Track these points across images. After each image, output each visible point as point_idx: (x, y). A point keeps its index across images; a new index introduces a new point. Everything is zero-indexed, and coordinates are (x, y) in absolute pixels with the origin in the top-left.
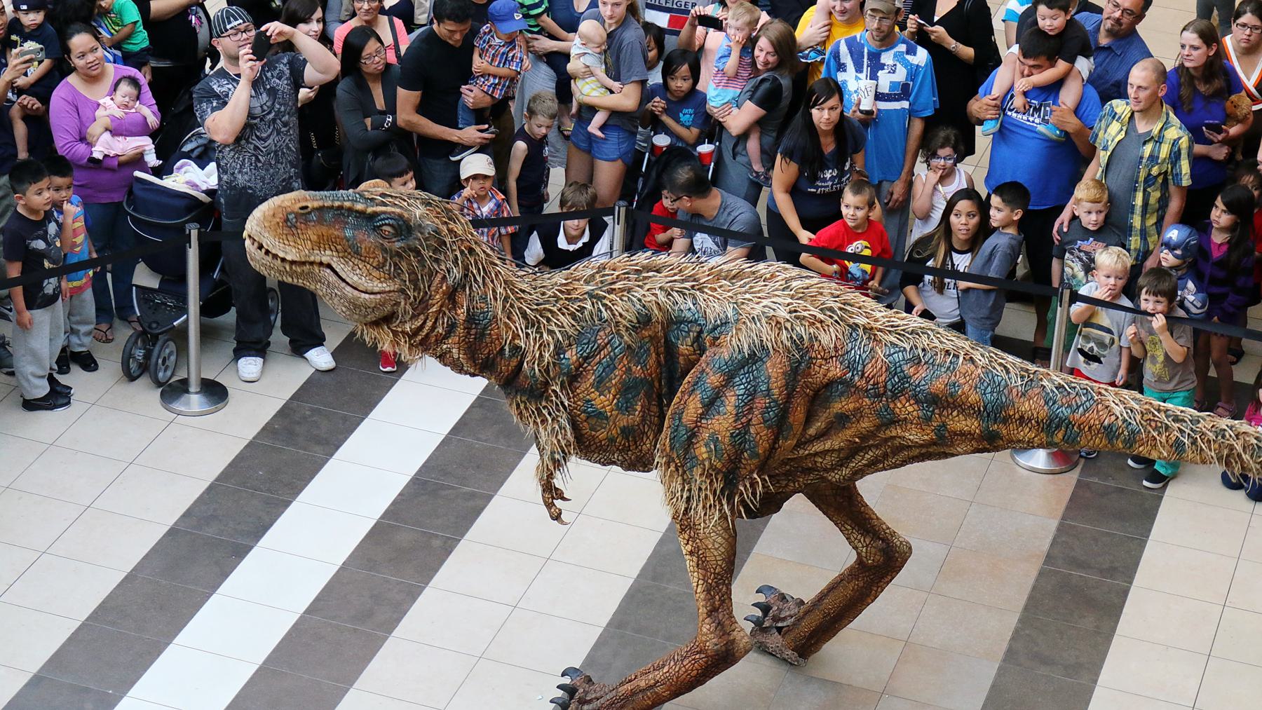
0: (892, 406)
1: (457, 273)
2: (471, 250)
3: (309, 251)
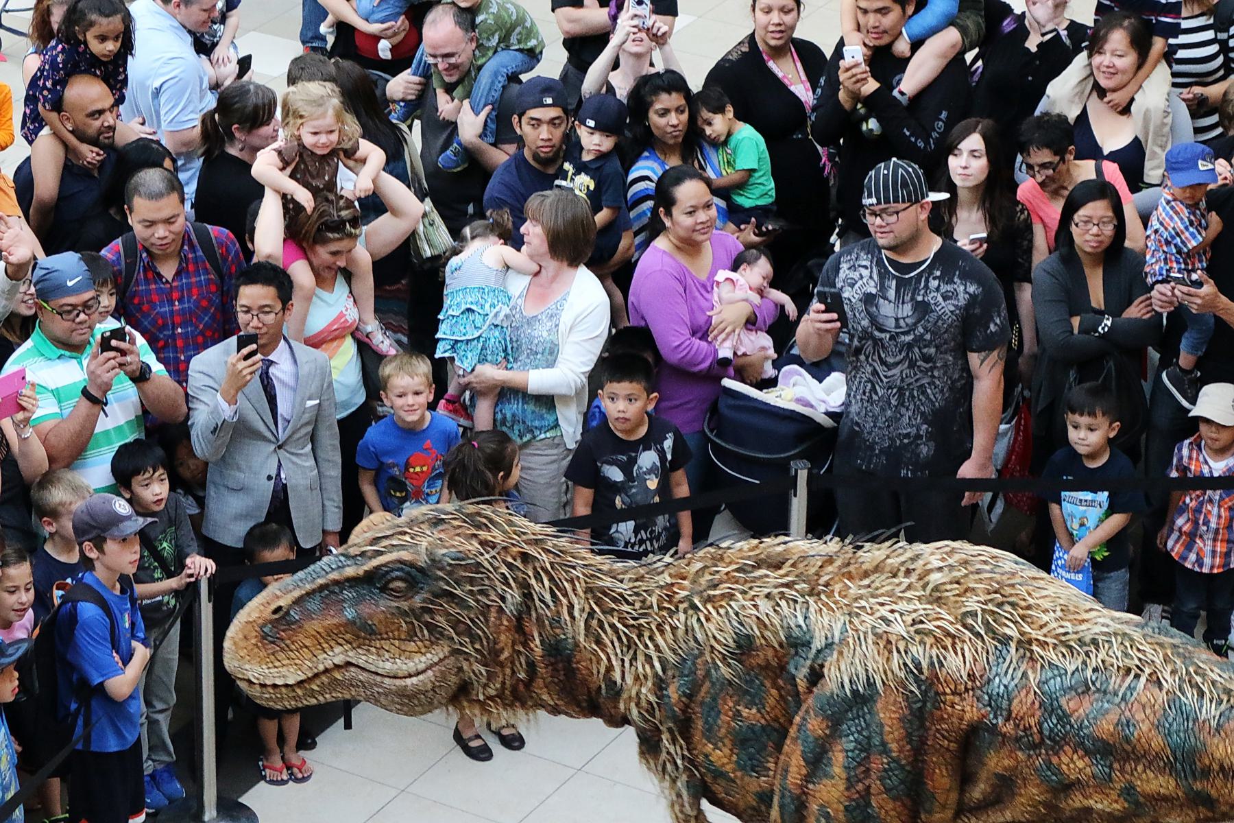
0: (1055, 760)
1: (514, 596)
2: (525, 557)
3: (310, 660)
